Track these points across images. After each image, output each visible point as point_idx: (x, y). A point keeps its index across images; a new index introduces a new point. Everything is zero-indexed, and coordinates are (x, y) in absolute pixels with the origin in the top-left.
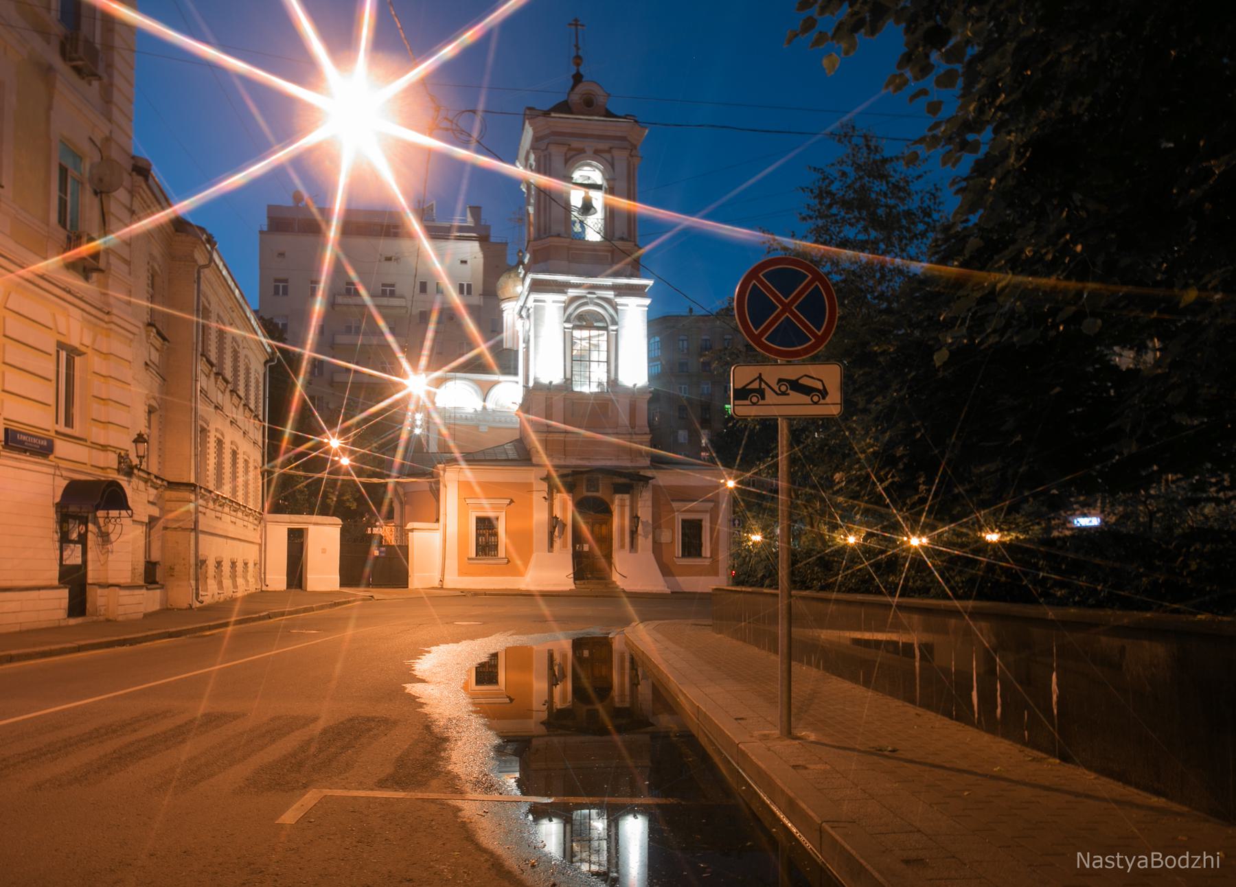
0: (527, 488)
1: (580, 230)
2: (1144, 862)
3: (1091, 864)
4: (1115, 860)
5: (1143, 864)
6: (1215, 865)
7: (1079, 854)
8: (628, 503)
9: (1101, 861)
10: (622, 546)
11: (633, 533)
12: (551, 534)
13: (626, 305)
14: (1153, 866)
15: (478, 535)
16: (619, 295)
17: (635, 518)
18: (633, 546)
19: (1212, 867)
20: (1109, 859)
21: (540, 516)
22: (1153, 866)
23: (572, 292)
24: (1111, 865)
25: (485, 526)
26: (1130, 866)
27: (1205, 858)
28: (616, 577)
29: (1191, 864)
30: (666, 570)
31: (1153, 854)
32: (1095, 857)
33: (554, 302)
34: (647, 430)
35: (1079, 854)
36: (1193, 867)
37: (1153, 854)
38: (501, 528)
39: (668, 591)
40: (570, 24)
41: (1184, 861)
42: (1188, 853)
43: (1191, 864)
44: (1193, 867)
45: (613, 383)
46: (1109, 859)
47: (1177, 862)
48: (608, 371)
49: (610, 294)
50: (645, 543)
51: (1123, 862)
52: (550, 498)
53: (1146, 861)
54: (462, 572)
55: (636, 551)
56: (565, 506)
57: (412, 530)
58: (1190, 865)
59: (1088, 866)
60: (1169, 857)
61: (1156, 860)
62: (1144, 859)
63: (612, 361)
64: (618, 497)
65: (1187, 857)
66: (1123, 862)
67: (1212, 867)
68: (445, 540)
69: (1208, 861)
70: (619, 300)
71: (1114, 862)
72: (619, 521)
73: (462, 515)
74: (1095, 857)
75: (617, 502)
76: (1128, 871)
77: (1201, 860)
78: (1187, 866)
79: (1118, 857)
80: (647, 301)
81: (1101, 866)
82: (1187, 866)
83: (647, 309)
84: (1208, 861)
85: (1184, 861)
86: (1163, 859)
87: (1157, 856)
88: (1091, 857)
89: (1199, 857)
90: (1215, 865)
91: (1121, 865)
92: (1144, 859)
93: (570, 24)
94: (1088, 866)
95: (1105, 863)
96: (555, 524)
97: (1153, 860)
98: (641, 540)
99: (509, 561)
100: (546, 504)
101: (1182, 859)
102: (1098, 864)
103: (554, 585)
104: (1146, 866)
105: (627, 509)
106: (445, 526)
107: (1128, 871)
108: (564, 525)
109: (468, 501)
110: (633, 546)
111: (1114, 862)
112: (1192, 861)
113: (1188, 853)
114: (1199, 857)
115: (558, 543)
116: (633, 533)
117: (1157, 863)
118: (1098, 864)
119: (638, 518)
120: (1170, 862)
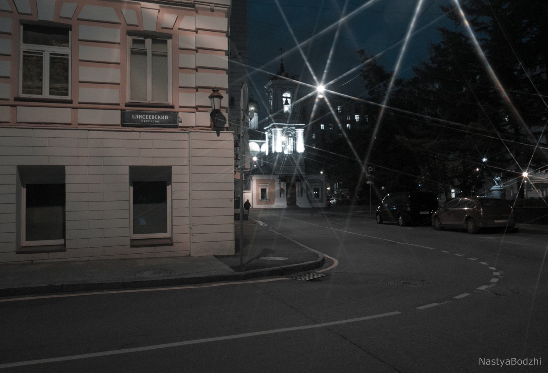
0: (274, 181)
1: (383, 223)
2: (508, 362)
3: (485, 363)
4: (496, 361)
5: (508, 363)
6: (539, 363)
7: (480, 359)
8: (300, 184)
9: (490, 362)
10: (299, 195)
11: (301, 192)
12: (280, 193)
13: (298, 131)
14: (512, 364)
15: (261, 194)
16: (296, 128)
17: (302, 188)
18: (301, 196)
19: (538, 364)
20: (493, 361)
21: (277, 188)
22: (512, 364)
23: (284, 128)
24: (494, 363)
25: (263, 191)
26: (502, 364)
27: (534, 360)
28: (297, 204)
29: (528, 363)
30: (310, 202)
31: (512, 358)
32: (487, 360)
33: (280, 130)
34: (304, 164)
35: (480, 359)
36: (529, 364)
37: (512, 358)
38: (267, 191)
39: (311, 207)
40: (280, 50)
41: (526, 362)
42: (527, 358)
43: (528, 363)
44: (529, 364)
45: (295, 152)
46: (493, 361)
47: (522, 362)
48: (294, 149)
49: (294, 128)
50: (304, 194)
51: (499, 362)
52: (280, 184)
53: (509, 362)
54: (258, 204)
55: (302, 197)
56: (283, 185)
57: (244, 193)
58: (528, 364)
59: (484, 364)
60: (519, 360)
61: (513, 361)
62: (508, 361)
63: (295, 145)
64: (297, 182)
65: (527, 360)
66: (499, 362)
67: (538, 364)
68: (253, 195)
69: (536, 361)
70: (296, 130)
71: (495, 362)
72: (297, 189)
73: (257, 188)
74: (487, 360)
75: (297, 184)
76: (501, 366)
77: (533, 361)
78: (527, 364)
79: (497, 360)
80: (303, 130)
81: (490, 364)
82: (527, 364)
83: (303, 132)
84: (536, 361)
85: (526, 362)
86: (517, 361)
87: (514, 360)
88: (485, 360)
89: (532, 360)
90: (539, 363)
91: (498, 364)
92: (508, 361)
93: (280, 50)
94: (484, 364)
95: (491, 363)
96: (282, 190)
97: (512, 361)
98: (303, 194)
99: (269, 201)
100: (279, 185)
101: (525, 361)
102: (488, 363)
103: (282, 206)
104: (509, 364)
105: (300, 186)
106: (253, 191)
107: (501, 366)
108: (284, 190)
109: (259, 185)
110: (301, 196)
111: (495, 362)
112: (529, 362)
113: (527, 358)
114: (532, 360)
115: (282, 195)
116: (301, 192)
117: (514, 363)
118: (488, 363)
119: (303, 188)
120: (520, 362)
